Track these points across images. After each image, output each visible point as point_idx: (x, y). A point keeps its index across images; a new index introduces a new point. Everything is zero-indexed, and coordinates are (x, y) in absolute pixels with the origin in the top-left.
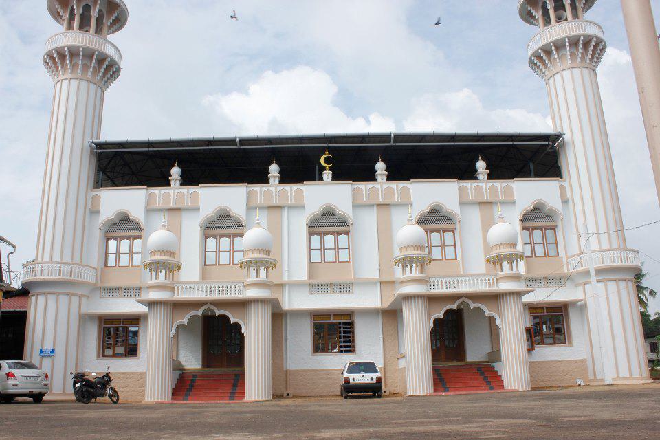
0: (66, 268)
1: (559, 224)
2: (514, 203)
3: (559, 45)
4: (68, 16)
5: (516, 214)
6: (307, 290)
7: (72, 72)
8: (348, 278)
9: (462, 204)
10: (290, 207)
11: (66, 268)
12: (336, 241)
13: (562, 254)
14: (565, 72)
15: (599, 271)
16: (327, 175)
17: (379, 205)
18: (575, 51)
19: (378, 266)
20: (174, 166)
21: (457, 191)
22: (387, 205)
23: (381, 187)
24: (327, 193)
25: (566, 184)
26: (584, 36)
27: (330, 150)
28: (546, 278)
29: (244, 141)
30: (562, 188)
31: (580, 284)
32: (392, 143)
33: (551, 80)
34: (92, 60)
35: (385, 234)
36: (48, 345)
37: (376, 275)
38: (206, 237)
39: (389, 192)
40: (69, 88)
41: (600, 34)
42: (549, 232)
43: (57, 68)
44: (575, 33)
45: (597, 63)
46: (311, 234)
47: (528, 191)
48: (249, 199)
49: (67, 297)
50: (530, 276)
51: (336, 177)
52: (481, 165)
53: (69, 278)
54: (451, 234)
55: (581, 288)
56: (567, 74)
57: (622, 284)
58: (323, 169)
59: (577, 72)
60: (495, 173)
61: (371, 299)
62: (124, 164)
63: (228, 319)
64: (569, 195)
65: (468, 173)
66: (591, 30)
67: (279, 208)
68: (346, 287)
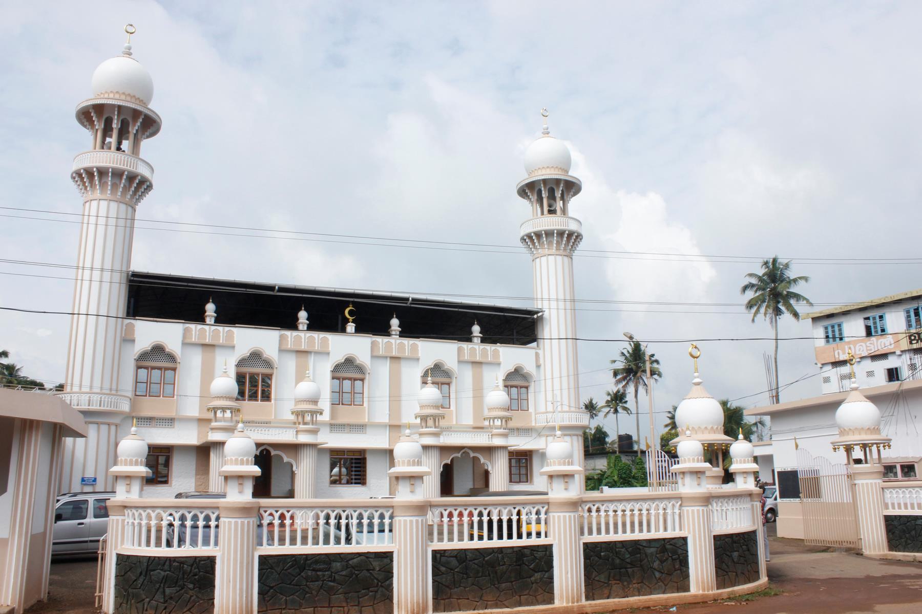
0: (96, 398)
1: (454, 381)
2: (499, 364)
3: (549, 234)
4: (536, 197)
5: (500, 375)
6: (328, 429)
7: (111, 193)
8: (172, 414)
9: (373, 357)
10: (317, 353)
11: (96, 398)
12: (353, 386)
13: (531, 409)
14: (101, 202)
15: (562, 428)
16: (351, 327)
17: (392, 358)
18: (118, 182)
19: (388, 412)
20: (208, 302)
21: (278, 339)
22: (213, 346)
23: (394, 342)
24: (350, 344)
25: (540, 352)
26: (129, 172)
27: (354, 303)
28: (518, 429)
29: (282, 289)
30: (537, 355)
31: (543, 436)
32: (408, 305)
33: (538, 260)
34: (121, 179)
35: (208, 375)
36: (90, 474)
37: (385, 420)
38: (139, 367)
39: (401, 347)
40: (101, 207)
41: (580, 231)
42: (523, 390)
43: (84, 183)
44: (122, 166)
45: (138, 200)
46: (139, 367)
47: (510, 356)
48: (184, 337)
49: (96, 426)
50: (333, 422)
51: (359, 330)
52: (395, 323)
53: (98, 408)
54: (361, 382)
55: (543, 439)
56: (551, 258)
57: (575, 438)
58: (347, 321)
59: (559, 258)
60: (407, 331)
61: (188, 436)
62: (152, 296)
63: (479, 460)
64: (541, 362)
65: (383, 330)
66: (573, 226)
67: (212, 346)
68: (360, 428)
